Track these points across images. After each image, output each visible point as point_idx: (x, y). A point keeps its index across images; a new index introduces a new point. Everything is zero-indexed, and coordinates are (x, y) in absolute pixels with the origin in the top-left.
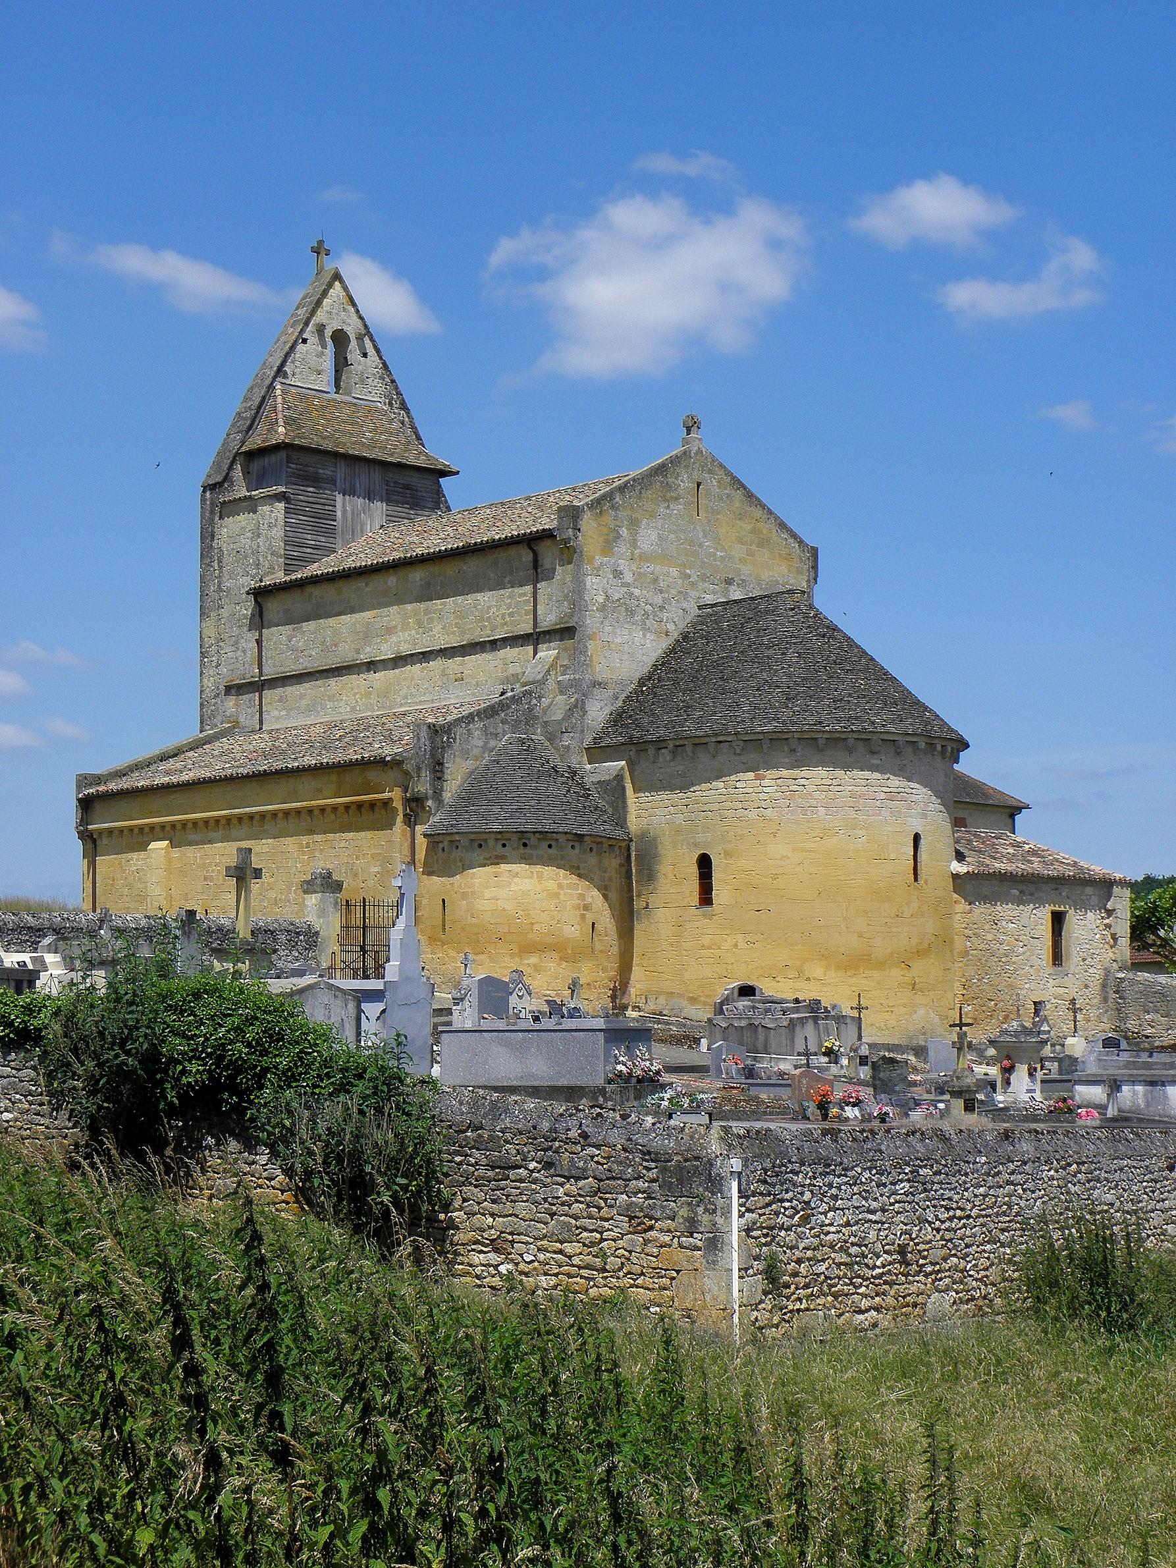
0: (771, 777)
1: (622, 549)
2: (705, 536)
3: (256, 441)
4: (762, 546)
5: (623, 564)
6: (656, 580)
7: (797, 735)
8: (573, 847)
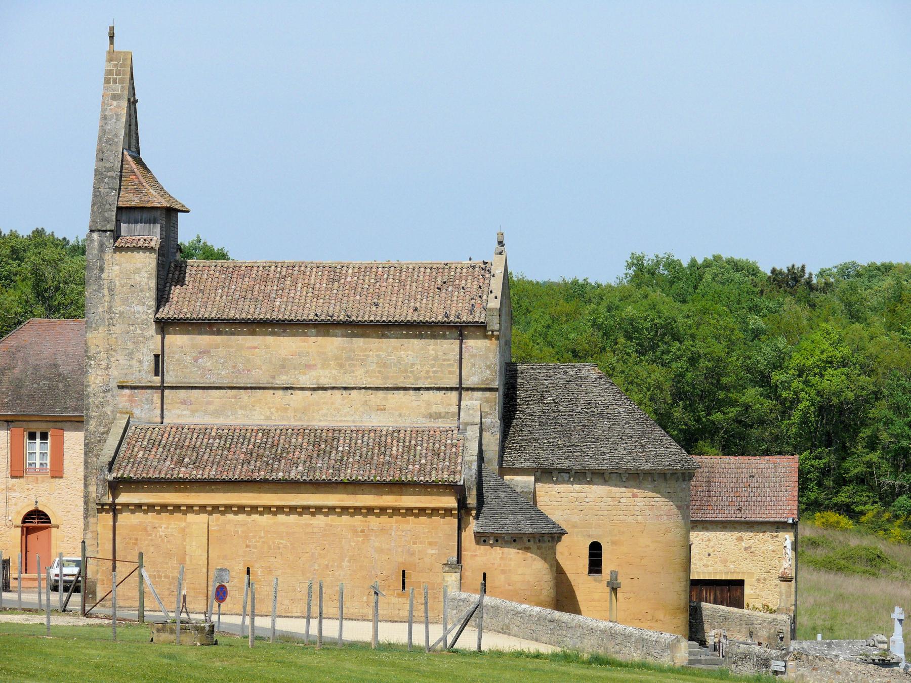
0: (641, 496)
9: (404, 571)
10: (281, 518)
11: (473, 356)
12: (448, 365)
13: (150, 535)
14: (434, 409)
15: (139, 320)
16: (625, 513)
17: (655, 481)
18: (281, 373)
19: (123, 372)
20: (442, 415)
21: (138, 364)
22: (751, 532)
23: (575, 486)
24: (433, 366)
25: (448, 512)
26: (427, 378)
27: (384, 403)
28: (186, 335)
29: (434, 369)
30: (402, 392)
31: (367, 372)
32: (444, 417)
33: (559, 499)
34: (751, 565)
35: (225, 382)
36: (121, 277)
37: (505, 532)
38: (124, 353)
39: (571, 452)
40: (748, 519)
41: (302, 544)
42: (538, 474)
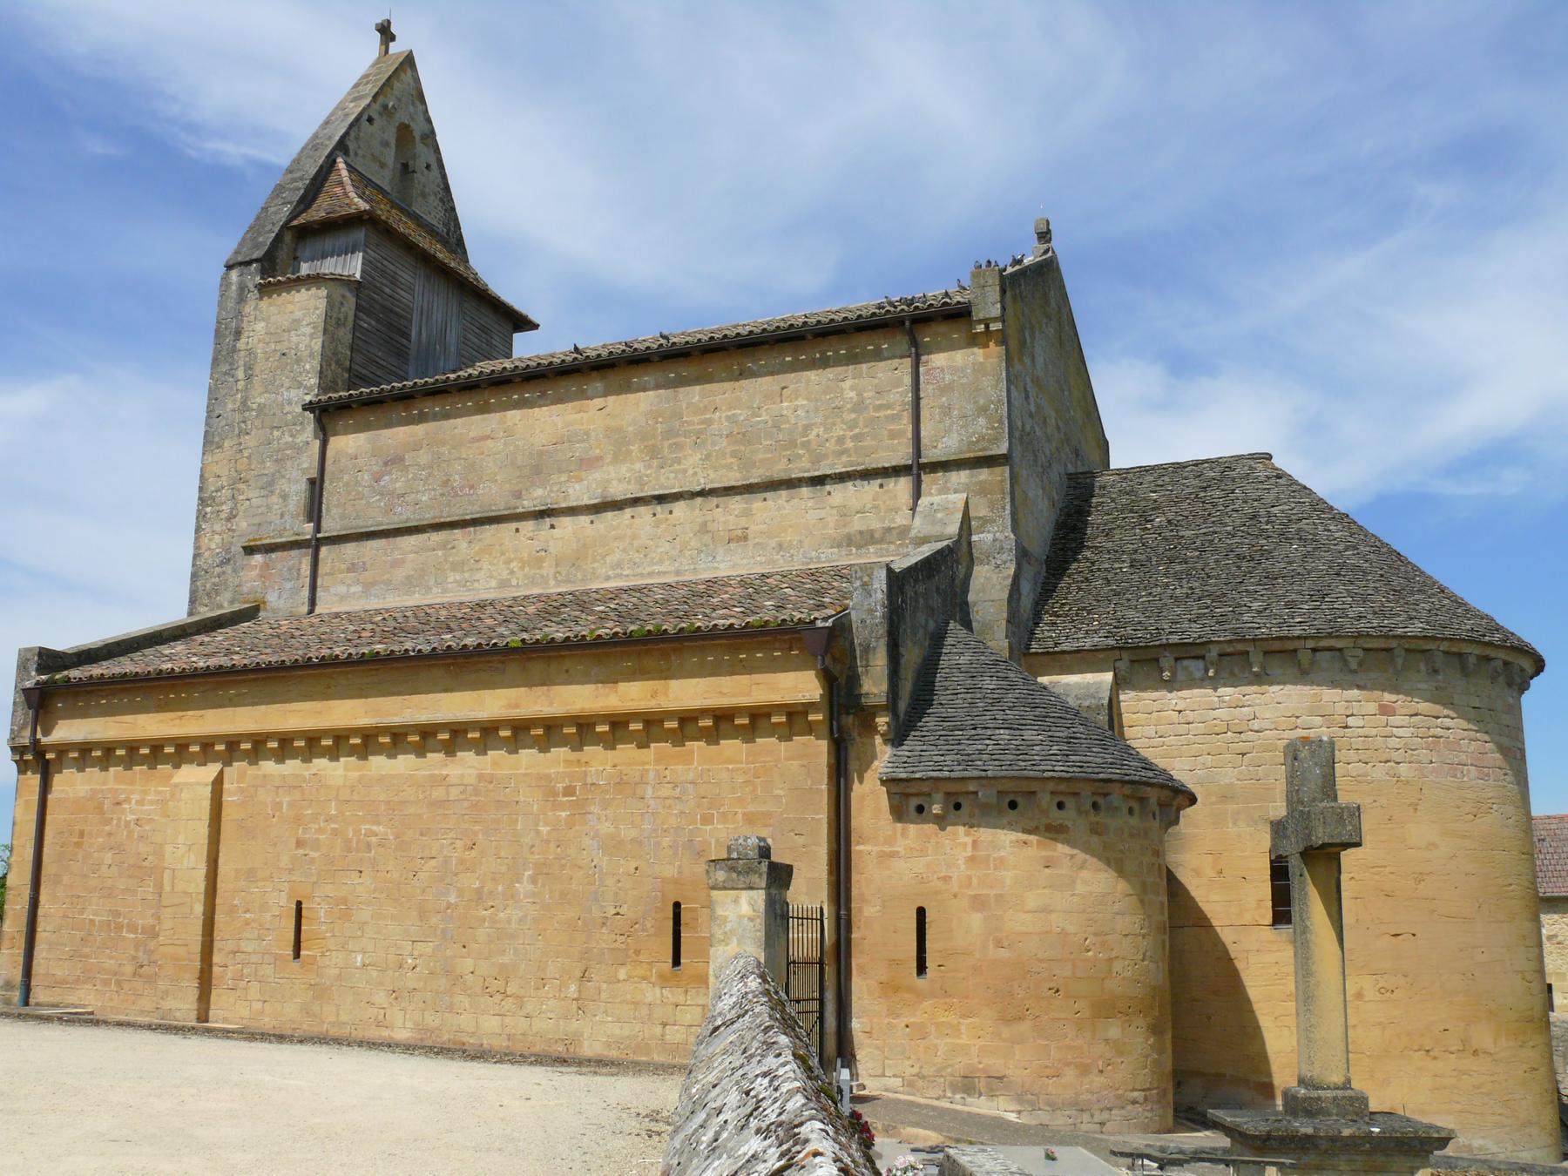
3: (317, 212)
7: (1444, 646)
9: (677, 905)
10: (378, 763)
11: (945, 390)
12: (887, 417)
13: (108, 822)
14: (857, 524)
15: (290, 417)
16: (1363, 755)
17: (1436, 671)
18: (533, 484)
19: (257, 520)
20: (877, 535)
21: (281, 501)
22: (1555, 913)
23: (1222, 691)
24: (852, 425)
25: (794, 718)
26: (841, 453)
27: (743, 522)
28: (363, 431)
29: (857, 431)
30: (784, 493)
31: (708, 457)
32: (882, 541)
33: (1183, 728)
34: (1560, 962)
35: (428, 517)
36: (267, 340)
37: (976, 773)
38: (260, 484)
39: (1207, 608)
40: (1548, 895)
41: (421, 834)
42: (1123, 665)
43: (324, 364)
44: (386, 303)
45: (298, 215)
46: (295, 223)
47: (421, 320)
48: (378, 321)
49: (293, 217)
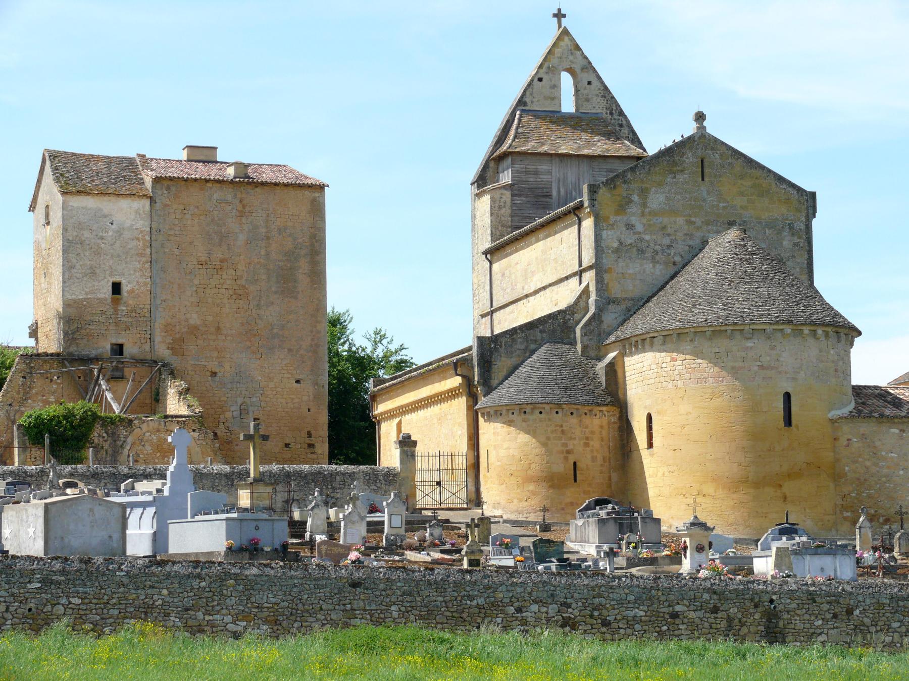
1: (634, 209)
2: (709, 193)
4: (763, 196)
5: (634, 220)
6: (664, 228)
7: (692, 330)
8: (557, 413)
25: (451, 395)
43: (493, 230)
44: (532, 186)
45: (493, 154)
46: (495, 155)
47: (559, 184)
48: (526, 196)
49: (493, 152)
